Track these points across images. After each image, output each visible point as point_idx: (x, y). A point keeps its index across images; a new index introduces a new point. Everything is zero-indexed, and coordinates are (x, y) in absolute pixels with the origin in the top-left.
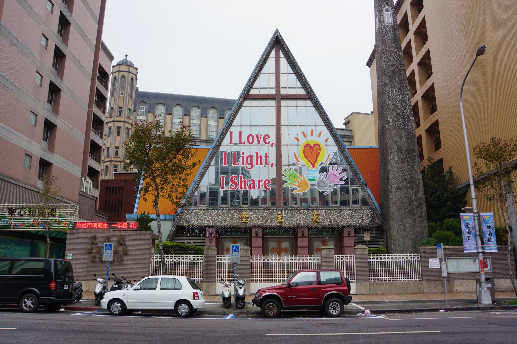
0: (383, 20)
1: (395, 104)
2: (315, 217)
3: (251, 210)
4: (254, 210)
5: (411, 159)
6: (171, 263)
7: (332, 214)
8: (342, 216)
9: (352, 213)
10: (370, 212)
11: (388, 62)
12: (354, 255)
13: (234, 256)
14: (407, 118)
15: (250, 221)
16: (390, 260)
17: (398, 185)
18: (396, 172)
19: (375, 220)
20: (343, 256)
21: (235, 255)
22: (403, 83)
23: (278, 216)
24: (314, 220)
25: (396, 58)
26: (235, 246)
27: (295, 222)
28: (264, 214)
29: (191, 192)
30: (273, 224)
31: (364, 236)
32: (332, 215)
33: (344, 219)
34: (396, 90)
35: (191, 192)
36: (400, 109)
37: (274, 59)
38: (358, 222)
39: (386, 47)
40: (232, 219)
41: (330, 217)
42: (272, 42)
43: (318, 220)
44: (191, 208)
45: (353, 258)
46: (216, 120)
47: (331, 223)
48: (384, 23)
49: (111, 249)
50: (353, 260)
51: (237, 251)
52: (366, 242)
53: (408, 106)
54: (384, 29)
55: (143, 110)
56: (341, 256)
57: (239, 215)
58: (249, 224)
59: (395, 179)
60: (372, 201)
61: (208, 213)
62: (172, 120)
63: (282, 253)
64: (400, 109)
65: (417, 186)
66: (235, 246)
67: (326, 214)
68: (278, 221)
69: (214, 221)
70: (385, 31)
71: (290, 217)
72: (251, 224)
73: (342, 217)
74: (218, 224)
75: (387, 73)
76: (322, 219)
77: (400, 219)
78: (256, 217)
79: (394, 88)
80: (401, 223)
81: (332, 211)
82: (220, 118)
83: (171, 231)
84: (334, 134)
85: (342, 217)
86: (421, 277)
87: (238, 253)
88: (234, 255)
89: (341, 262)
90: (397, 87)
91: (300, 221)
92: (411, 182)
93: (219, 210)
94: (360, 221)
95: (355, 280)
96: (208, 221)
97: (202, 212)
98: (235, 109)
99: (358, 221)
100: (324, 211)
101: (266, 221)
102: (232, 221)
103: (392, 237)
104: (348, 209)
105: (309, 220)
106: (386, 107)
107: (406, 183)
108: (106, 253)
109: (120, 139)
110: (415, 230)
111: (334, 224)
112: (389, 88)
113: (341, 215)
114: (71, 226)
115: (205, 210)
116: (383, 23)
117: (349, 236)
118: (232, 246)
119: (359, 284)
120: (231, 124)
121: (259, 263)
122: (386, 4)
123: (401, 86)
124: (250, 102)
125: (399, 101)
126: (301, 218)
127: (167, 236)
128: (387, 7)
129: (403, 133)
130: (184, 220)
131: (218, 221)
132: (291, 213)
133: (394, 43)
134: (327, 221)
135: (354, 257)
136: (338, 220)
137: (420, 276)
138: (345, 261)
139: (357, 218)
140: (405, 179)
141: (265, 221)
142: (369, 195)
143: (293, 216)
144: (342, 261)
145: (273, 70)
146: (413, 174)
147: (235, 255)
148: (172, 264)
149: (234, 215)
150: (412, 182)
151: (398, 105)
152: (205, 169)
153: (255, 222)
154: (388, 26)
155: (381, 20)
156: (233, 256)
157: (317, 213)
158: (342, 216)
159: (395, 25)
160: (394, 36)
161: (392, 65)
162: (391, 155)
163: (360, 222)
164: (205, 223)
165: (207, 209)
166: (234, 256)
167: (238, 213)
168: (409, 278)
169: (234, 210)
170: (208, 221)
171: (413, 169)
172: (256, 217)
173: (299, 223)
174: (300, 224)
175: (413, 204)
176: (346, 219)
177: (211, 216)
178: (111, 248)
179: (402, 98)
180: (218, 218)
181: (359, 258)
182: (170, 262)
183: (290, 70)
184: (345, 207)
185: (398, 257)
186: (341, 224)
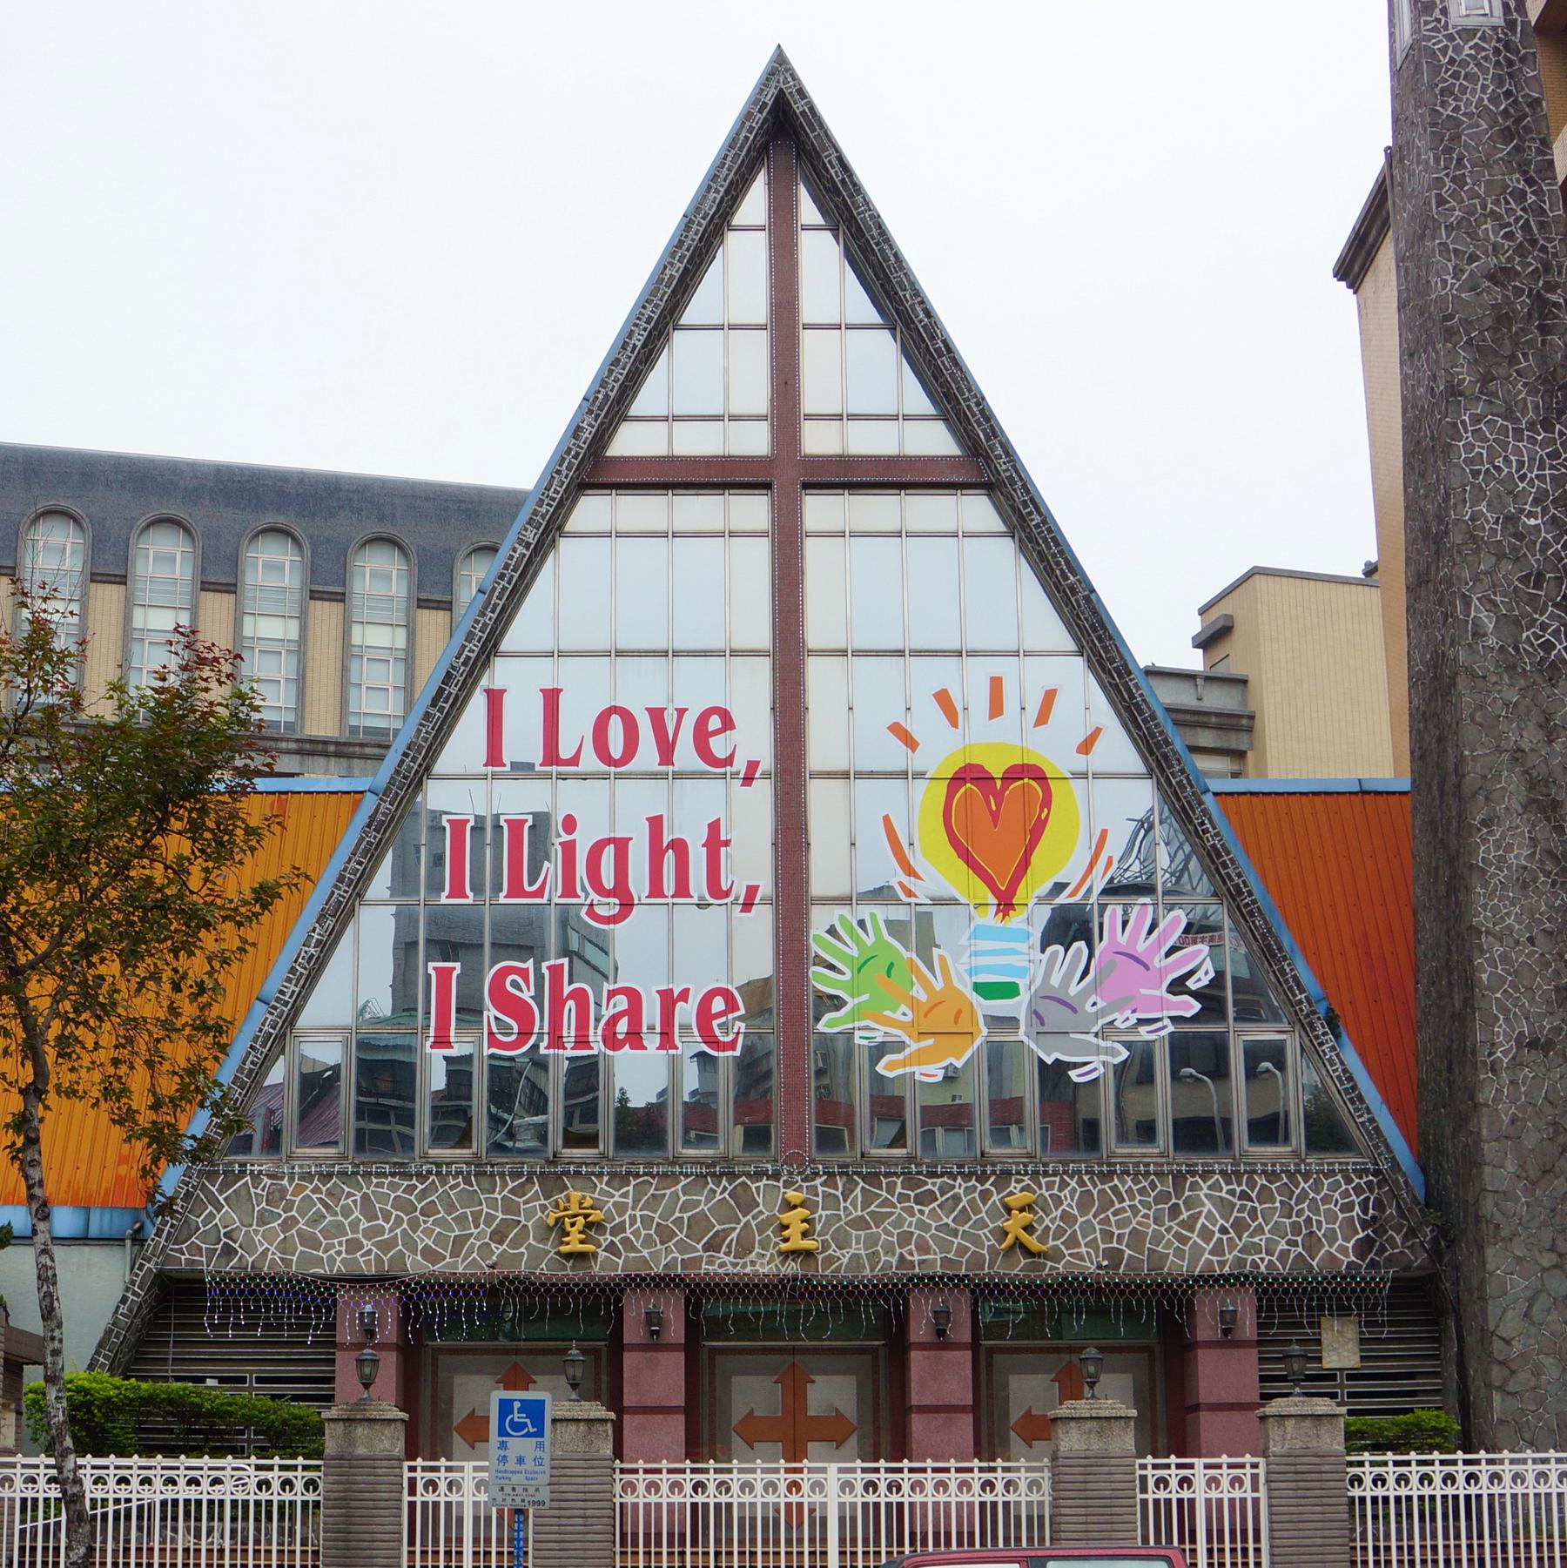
1: (1511, 520)
2: (1014, 1224)
3: (619, 1179)
4: (637, 1175)
6: (123, 1506)
7: (1122, 1200)
8: (1185, 1216)
9: (1244, 1196)
10: (1358, 1190)
11: (1473, 258)
12: (1261, 1461)
13: (511, 1464)
15: (611, 1249)
18: (1517, 943)
19: (1391, 1240)
20: (1191, 1466)
21: (520, 1460)
23: (786, 1217)
26: (517, 1405)
28: (696, 1204)
29: (248, 1066)
30: (753, 1263)
31: (1319, 1342)
32: (1123, 1210)
33: (1195, 1236)
34: (1518, 433)
35: (248, 1066)
36: (1543, 551)
37: (761, 238)
38: (1284, 1255)
39: (1460, 160)
40: (498, 1236)
41: (1106, 1221)
42: (751, 130)
43: (1032, 1242)
44: (242, 1165)
45: (1255, 1477)
46: (399, 616)
47: (1114, 1256)
48: (1444, 11)
50: (1255, 1489)
51: (528, 1435)
52: (1332, 1377)
54: (1444, 50)
56: (1179, 1466)
57: (543, 1208)
58: (607, 1266)
59: (1514, 986)
60: (1372, 1120)
61: (352, 1197)
62: (127, 618)
63: (810, 1445)
64: (1543, 551)
66: (517, 1405)
67: (1085, 1202)
68: (784, 1246)
69: (386, 1246)
70: (1452, 61)
71: (860, 1223)
72: (619, 1266)
73: (1182, 1224)
74: (415, 1265)
75: (1467, 323)
76: (1059, 1232)
77: (1547, 1235)
78: (647, 1221)
79: (1508, 415)
81: (1124, 1183)
82: (423, 604)
83: (124, 1309)
84: (1137, 706)
85: (1182, 1224)
87: (540, 1446)
88: (512, 1459)
89: (1180, 1501)
90: (1524, 412)
91: (923, 1248)
93: (419, 1175)
94: (1295, 1244)
96: (354, 1246)
97: (316, 1190)
98: (521, 549)
99: (1283, 1246)
100: (1073, 1183)
102: (498, 1249)
105: (976, 1241)
111: (1134, 1263)
112: (1476, 419)
113: (1175, 1211)
115: (330, 1175)
116: (1437, 13)
117: (1228, 1338)
120: (496, 645)
123: (1548, 409)
124: (613, 508)
125: (1536, 502)
130: (204, 1240)
131: (411, 1244)
132: (868, 1199)
133: (1507, 135)
134: (1092, 1244)
135: (1261, 1471)
139: (1278, 1229)
141: (707, 1248)
143: (879, 1218)
145: (755, 304)
148: (128, 1517)
149: (509, 1207)
151: (1532, 522)
152: (330, 923)
153: (645, 1253)
154: (1468, 33)
156: (508, 1467)
157: (1028, 1197)
158: (1185, 1216)
160: (1508, 94)
161: (1491, 277)
164: (333, 1259)
166: (511, 1464)
167: (536, 1198)
169: (515, 1175)
170: (354, 1246)
172: (647, 1221)
173: (916, 1258)
174: (921, 1263)
176: (1206, 1234)
180: (414, 1225)
182: (117, 1501)
183: (861, 307)
184: (1200, 1160)
185: (1530, 1470)
186: (1178, 1264)
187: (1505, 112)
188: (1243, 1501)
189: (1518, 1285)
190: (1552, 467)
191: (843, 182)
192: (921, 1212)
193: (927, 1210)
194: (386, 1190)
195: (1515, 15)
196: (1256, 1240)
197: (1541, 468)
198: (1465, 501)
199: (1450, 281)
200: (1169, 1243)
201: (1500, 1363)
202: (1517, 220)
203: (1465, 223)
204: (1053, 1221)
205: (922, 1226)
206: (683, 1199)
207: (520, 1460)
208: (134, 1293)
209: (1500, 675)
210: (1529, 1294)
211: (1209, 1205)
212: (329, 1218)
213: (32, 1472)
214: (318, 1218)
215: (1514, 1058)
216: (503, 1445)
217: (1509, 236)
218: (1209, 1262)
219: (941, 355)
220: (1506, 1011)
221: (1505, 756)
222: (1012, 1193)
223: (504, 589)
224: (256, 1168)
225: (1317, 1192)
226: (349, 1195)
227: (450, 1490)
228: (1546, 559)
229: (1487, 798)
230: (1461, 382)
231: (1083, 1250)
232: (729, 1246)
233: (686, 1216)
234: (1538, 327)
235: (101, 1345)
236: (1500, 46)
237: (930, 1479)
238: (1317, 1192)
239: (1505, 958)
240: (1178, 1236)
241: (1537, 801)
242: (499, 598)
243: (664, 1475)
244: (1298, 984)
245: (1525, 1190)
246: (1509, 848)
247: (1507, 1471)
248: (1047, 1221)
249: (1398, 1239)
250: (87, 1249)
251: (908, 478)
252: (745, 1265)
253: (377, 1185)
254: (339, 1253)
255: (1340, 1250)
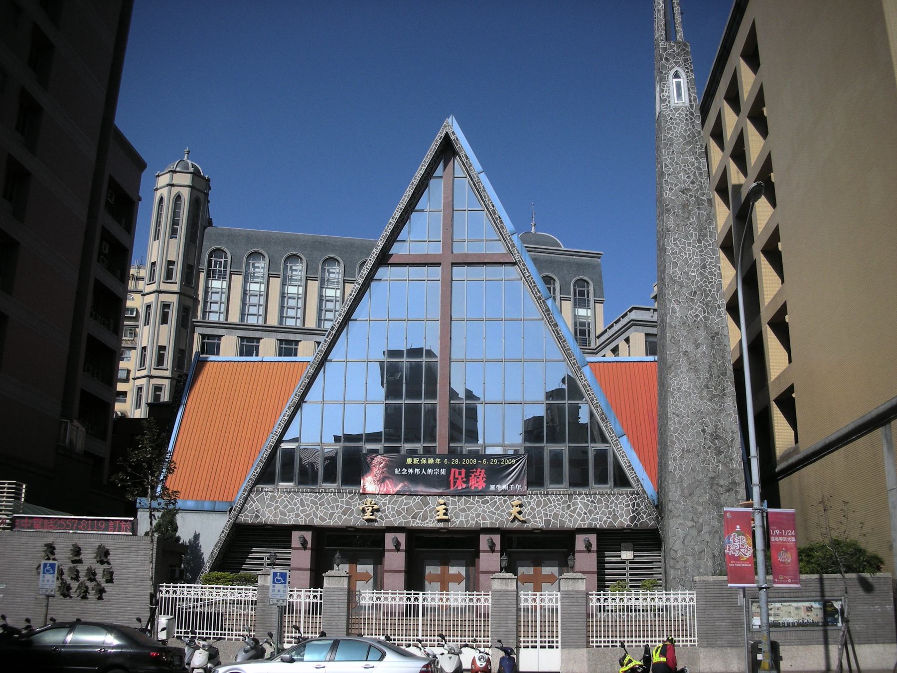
0: (668, 97)
1: (687, 273)
5: (716, 389)
6: (210, 601)
7: (551, 503)
8: (572, 508)
9: (593, 502)
11: (676, 185)
12: (559, 593)
13: (276, 592)
14: (711, 301)
15: (381, 518)
16: (672, 603)
17: (687, 444)
18: (683, 417)
19: (642, 517)
20: (301, 591)
21: (279, 591)
22: (706, 229)
23: (438, 508)
24: (512, 517)
25: (692, 177)
26: (48, 565)
27: (473, 519)
29: (265, 456)
30: (427, 523)
33: (575, 515)
34: (690, 244)
35: (265, 456)
36: (696, 284)
38: (605, 522)
39: (673, 152)
40: (344, 513)
43: (520, 517)
44: (262, 489)
45: (557, 599)
48: (669, 102)
49: (54, 573)
51: (281, 583)
53: (715, 275)
55: (220, 267)
56: (414, 594)
57: (359, 504)
58: (382, 523)
60: (636, 476)
61: (297, 499)
64: (696, 284)
65: (728, 446)
66: (48, 565)
68: (437, 518)
69: (307, 516)
71: (463, 510)
74: (317, 522)
77: (690, 515)
79: (686, 237)
80: (690, 524)
81: (552, 497)
83: (223, 535)
84: (560, 337)
85: (571, 511)
86: (696, 639)
87: (285, 587)
88: (276, 591)
91: (484, 519)
92: (715, 437)
95: (559, 644)
96: (297, 515)
99: (605, 518)
100: (535, 497)
101: (414, 517)
103: (672, 552)
104: (585, 494)
105: (502, 516)
106: (667, 280)
107: (705, 439)
108: (43, 581)
109: (141, 342)
110: (720, 538)
111: (555, 524)
112: (675, 240)
113: (569, 507)
114: (9, 524)
115: (290, 492)
116: (667, 103)
117: (492, 549)
118: (274, 573)
119: (566, 651)
121: (399, 605)
122: (675, 62)
123: (700, 236)
125: (695, 267)
126: (485, 512)
127: (214, 545)
128: (676, 68)
129: (702, 335)
130: (249, 512)
132: (466, 502)
134: (541, 518)
135: (559, 596)
136: (563, 516)
137: (694, 637)
138: (420, 603)
140: (704, 431)
141: (412, 518)
142: (630, 465)
143: (469, 509)
144: (416, 603)
146: (720, 421)
147: (279, 591)
148: (212, 604)
149: (348, 503)
150: (718, 437)
151: (693, 274)
153: (392, 519)
154: (676, 109)
155: (663, 96)
157: (520, 502)
158: (572, 508)
159: (691, 106)
160: (690, 130)
162: (675, 380)
163: (609, 520)
165: (294, 492)
166: (276, 592)
168: (632, 642)
170: (297, 515)
171: (721, 411)
172: (393, 509)
173: (482, 522)
174: (483, 523)
175: (717, 484)
176: (579, 515)
177: (303, 505)
178: (54, 570)
179: (703, 260)
180: (317, 509)
181: (567, 596)
182: (208, 600)
184: (578, 490)
186: (570, 524)
187: (689, 136)
188: (317, 603)
189: (680, 533)
190: (701, 255)
191: (466, 162)
192: (484, 507)
193: (485, 506)
194: (308, 497)
195: (693, 103)
196: (596, 516)
197: (697, 256)
198: (670, 267)
199: (668, 193)
200: (567, 517)
201: (673, 559)
202: (691, 172)
203: (674, 173)
204: (528, 510)
205: (484, 511)
206: (405, 501)
207: (48, 581)
208: (226, 530)
209: (681, 326)
210: (684, 535)
211: (580, 505)
212: (290, 506)
213: (645, 597)
214: (286, 506)
215: (681, 456)
216: (44, 577)
217: (689, 177)
218: (580, 524)
219: (497, 220)
220: (679, 440)
221: (681, 354)
222: (514, 501)
223: (351, 299)
224: (266, 489)
225: (617, 500)
226: (296, 498)
227: (477, 601)
228: (698, 287)
229: (675, 368)
230: (671, 227)
231: (538, 520)
232: (420, 517)
233: (406, 507)
234: (697, 208)
235: (216, 546)
236: (688, 113)
237: (390, 596)
238: (617, 500)
239: (679, 422)
240: (569, 515)
241: (691, 369)
242: (350, 302)
243: (390, 595)
244: (612, 430)
245: (683, 501)
246: (682, 385)
247: (680, 597)
248: (526, 510)
249: (645, 516)
250: (214, 514)
251: (486, 261)
252: (424, 524)
253: (305, 496)
254: (292, 518)
255: (624, 520)
